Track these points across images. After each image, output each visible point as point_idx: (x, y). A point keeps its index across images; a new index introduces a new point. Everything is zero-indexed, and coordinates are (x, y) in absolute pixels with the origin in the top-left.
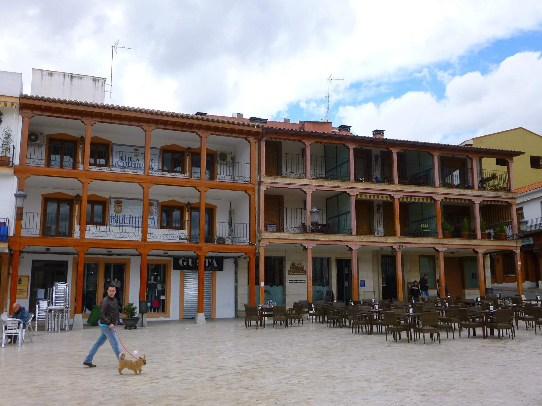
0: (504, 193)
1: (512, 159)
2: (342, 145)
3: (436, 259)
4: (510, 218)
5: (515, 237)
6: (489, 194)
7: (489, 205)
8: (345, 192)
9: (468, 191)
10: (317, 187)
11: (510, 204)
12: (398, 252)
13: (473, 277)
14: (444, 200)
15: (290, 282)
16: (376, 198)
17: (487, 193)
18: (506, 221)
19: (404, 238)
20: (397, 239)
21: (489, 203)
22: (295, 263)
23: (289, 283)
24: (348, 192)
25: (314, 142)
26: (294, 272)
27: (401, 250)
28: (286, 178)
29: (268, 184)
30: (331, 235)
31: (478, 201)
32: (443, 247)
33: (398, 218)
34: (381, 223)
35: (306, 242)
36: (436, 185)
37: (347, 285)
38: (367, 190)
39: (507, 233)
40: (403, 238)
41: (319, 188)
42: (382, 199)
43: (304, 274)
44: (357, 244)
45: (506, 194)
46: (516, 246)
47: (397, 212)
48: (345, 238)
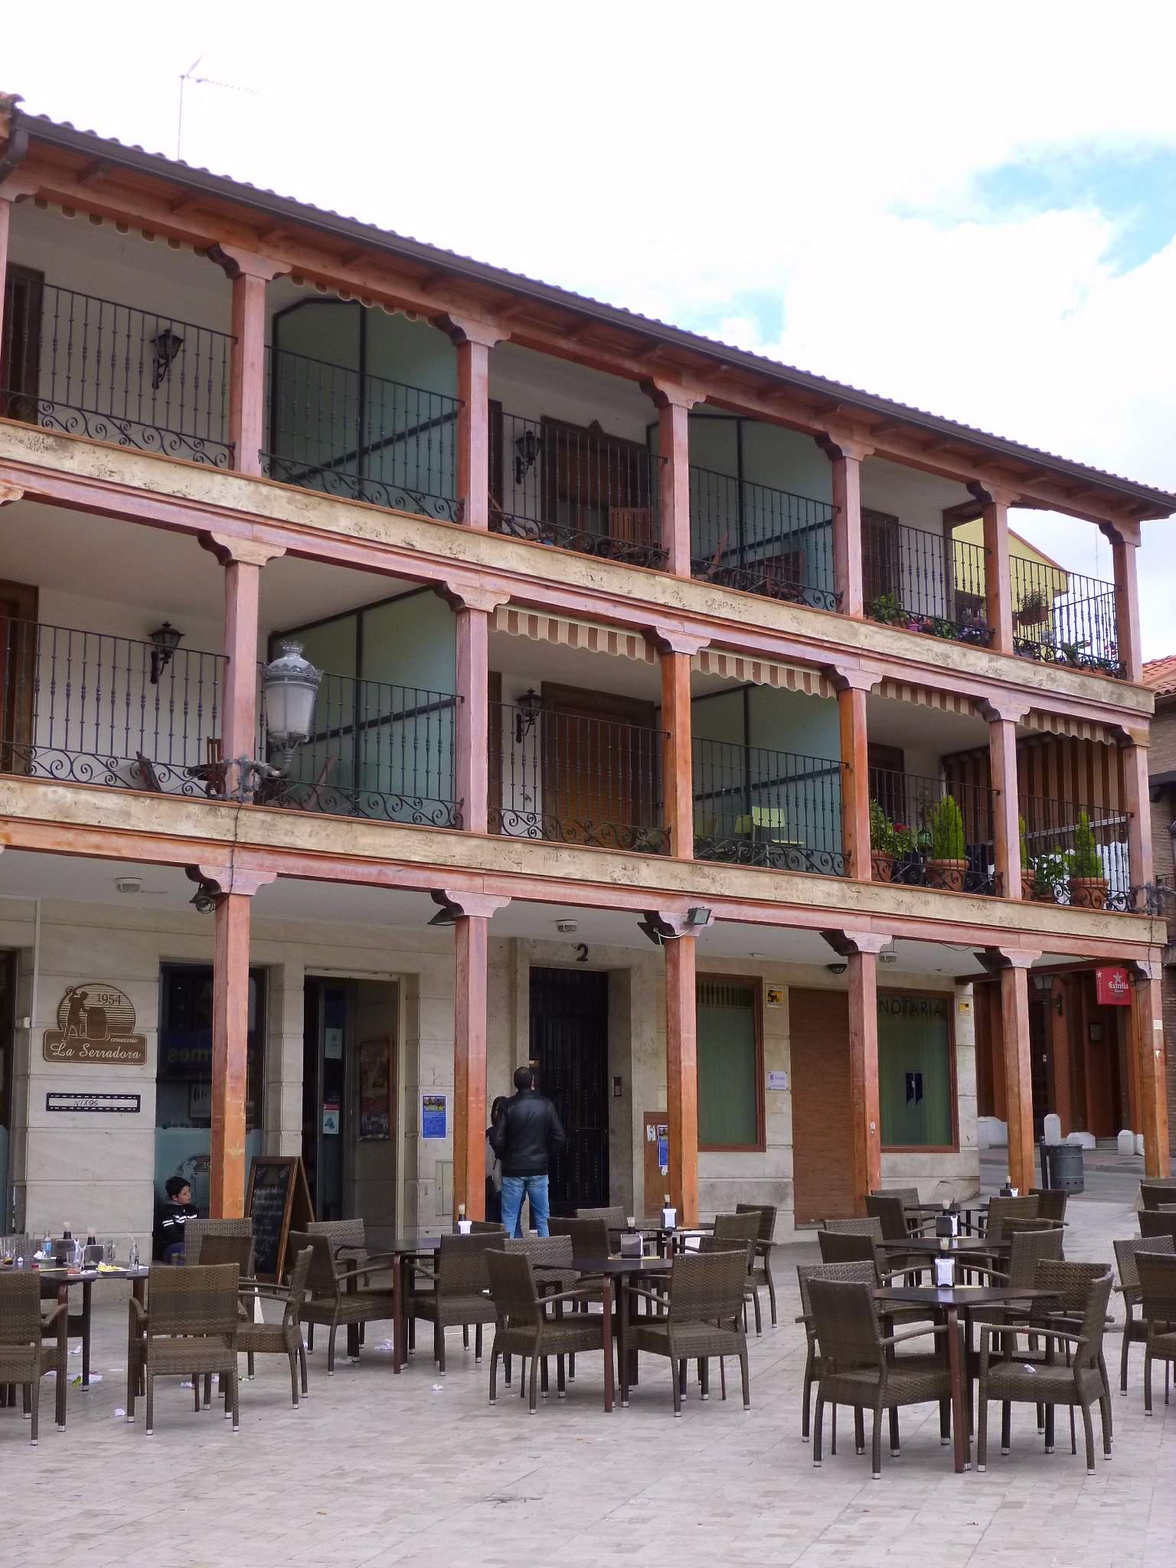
1: (1136, 533)
2: (426, 321)
3: (765, 997)
4: (1114, 804)
5: (1142, 898)
8: (437, 587)
9: (980, 658)
10: (293, 535)
12: (683, 943)
15: (54, 1103)
18: (1064, 830)
19: (713, 871)
20: (682, 870)
22: (86, 989)
23: (49, 1108)
24: (452, 587)
26: (76, 1045)
28: (125, 456)
29: (13, 476)
30: (362, 827)
31: (1012, 709)
33: (686, 762)
34: (530, 792)
35: (223, 854)
36: (852, 611)
37: (331, 1126)
38: (547, 587)
39: (1107, 877)
40: (706, 870)
41: (308, 544)
43: (136, 1055)
44: (490, 887)
45: (1117, 691)
46: (1150, 945)
47: (683, 725)
48: (435, 847)
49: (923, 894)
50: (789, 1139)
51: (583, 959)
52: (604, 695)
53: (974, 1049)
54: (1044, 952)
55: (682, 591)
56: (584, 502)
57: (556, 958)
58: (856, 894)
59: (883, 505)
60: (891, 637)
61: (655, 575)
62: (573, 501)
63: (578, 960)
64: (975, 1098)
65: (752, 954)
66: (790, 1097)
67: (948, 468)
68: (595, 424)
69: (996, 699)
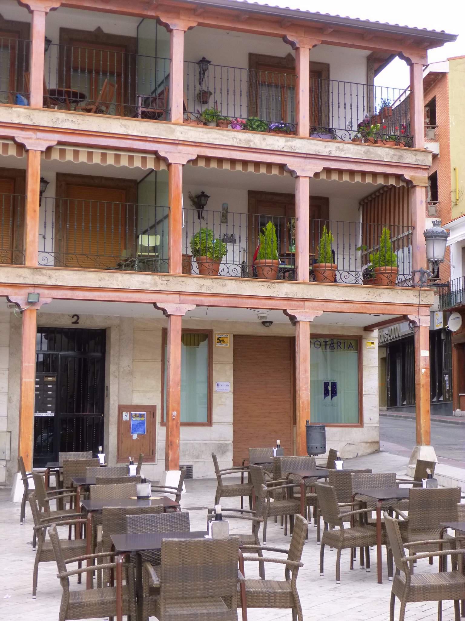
0: (392, 152)
5: (417, 277)
6: (342, 150)
7: (383, 187)
11: (409, 182)
13: (326, 393)
14: (323, 177)
16: (69, 157)
17: (338, 148)
21: (381, 181)
25: (194, 24)
27: (39, 308)
32: (181, 302)
42: (102, 160)
47: (33, 191)
49: (222, 281)
50: (230, 419)
51: (76, 322)
52: (101, 178)
53: (377, 368)
54: (324, 311)
55: (33, 115)
56: (97, 73)
57: (56, 323)
58: (165, 282)
59: (322, 58)
60: (203, 132)
61: (12, 107)
62: (90, 72)
63: (73, 323)
64: (378, 396)
65: (191, 317)
66: (232, 396)
67: (260, 30)
68: (99, 29)
69: (292, 163)
